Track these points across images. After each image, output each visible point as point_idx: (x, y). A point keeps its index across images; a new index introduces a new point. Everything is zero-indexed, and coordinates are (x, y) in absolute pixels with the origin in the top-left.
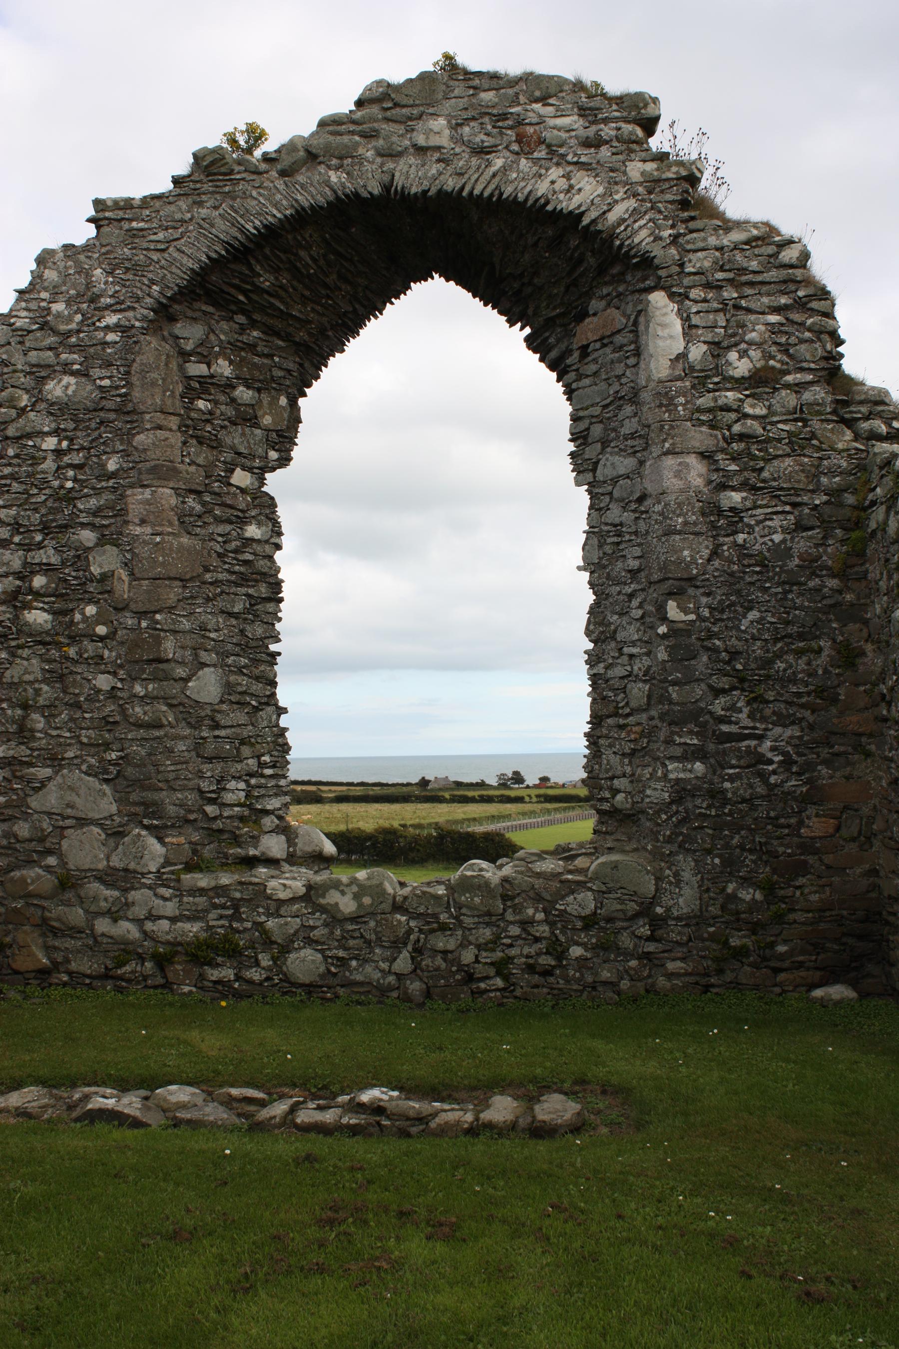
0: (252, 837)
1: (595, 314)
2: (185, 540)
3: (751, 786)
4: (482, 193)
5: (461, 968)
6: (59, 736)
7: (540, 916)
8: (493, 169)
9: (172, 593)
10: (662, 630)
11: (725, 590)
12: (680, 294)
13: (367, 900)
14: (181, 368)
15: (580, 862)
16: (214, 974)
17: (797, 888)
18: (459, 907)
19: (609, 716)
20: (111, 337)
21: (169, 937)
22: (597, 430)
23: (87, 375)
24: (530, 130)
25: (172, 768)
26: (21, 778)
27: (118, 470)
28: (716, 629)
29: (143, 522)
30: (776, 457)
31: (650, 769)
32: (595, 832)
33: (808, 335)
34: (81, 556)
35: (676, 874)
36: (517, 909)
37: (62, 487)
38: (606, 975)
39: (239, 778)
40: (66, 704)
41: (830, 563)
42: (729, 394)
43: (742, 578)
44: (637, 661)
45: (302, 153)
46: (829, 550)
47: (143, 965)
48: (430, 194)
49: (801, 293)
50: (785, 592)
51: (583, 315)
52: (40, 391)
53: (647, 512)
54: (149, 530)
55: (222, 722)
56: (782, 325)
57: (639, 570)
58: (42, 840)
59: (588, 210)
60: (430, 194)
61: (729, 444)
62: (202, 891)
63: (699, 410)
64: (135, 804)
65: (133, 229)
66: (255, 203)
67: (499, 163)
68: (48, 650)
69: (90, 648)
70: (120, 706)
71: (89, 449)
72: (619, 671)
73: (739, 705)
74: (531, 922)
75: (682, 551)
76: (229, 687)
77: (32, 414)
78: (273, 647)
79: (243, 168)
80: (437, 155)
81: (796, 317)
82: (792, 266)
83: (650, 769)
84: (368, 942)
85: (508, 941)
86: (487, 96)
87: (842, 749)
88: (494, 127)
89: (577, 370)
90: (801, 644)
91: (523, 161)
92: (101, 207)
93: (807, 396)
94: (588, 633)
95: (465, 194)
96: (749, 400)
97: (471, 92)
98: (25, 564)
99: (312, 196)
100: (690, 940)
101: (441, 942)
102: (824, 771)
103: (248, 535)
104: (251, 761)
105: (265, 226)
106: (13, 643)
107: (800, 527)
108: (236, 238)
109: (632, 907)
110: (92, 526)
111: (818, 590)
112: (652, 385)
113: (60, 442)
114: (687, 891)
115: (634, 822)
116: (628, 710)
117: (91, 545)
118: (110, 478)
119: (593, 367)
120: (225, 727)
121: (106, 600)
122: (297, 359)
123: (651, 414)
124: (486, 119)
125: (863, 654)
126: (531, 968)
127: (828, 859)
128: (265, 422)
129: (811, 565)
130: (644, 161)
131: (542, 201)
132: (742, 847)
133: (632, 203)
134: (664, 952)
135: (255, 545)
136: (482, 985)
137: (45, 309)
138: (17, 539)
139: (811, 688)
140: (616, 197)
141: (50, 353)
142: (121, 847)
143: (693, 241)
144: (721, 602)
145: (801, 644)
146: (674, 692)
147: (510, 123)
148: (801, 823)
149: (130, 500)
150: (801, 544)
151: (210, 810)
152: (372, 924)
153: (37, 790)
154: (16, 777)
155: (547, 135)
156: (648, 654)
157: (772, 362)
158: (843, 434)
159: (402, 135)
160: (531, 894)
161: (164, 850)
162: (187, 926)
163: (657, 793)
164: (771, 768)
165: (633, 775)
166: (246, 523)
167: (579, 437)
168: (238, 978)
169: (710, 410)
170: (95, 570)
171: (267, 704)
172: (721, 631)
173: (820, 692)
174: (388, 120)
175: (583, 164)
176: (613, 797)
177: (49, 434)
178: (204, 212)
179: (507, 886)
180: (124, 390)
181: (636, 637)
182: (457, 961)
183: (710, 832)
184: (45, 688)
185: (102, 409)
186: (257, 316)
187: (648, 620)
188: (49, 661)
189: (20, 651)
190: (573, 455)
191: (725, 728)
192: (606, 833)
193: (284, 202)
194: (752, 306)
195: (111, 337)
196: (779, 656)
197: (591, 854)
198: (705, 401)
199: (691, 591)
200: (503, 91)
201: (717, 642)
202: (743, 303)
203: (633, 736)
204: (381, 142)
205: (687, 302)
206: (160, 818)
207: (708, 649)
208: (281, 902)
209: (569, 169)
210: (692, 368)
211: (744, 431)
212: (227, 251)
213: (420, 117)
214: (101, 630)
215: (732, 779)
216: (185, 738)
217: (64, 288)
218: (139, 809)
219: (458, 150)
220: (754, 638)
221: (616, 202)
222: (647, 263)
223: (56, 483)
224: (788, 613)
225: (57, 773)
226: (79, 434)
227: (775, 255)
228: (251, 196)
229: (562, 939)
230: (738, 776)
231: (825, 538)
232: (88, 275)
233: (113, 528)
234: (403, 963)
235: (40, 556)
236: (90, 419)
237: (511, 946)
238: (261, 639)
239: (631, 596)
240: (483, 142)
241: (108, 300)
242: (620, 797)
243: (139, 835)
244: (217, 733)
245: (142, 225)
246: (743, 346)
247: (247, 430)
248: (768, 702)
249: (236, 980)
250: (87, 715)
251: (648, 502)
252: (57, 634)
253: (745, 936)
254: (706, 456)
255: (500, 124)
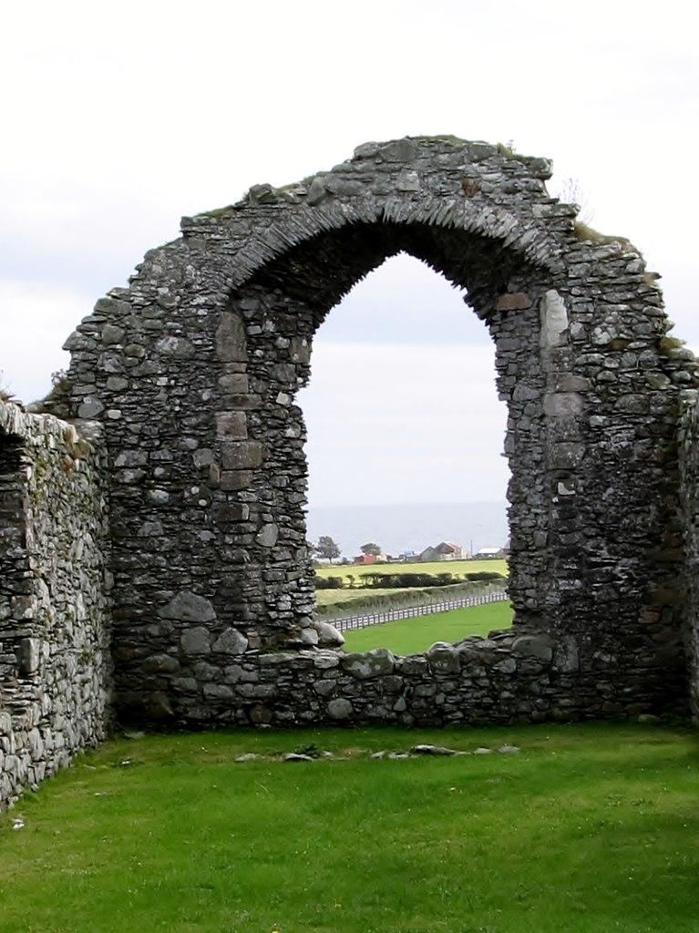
0: (297, 631)
1: (511, 293)
2: (253, 443)
3: (608, 594)
4: (441, 224)
5: (436, 706)
6: (177, 570)
7: (484, 674)
8: (448, 207)
9: (247, 478)
10: (555, 499)
11: (592, 476)
12: (565, 292)
13: (378, 667)
14: (246, 331)
15: (507, 641)
16: (282, 715)
17: (636, 654)
18: (434, 669)
19: (522, 551)
20: (201, 312)
21: (253, 694)
22: (513, 368)
23: (185, 337)
24: (471, 181)
25: (250, 589)
26: (151, 597)
27: (209, 399)
28: (587, 499)
29: (227, 433)
30: (624, 394)
31: (549, 584)
32: (514, 623)
33: (644, 318)
34: (188, 456)
35: (565, 647)
36: (469, 670)
37: (172, 410)
38: (524, 707)
39: (287, 593)
40: (181, 550)
41: (656, 459)
42: (596, 355)
43: (603, 468)
44: (540, 518)
45: (324, 192)
46: (655, 451)
47: (236, 712)
48: (408, 223)
49: (640, 291)
50: (629, 477)
51: (503, 290)
52: (154, 347)
53: (545, 426)
54: (231, 438)
55: (278, 558)
56: (629, 311)
57: (541, 461)
58: (166, 637)
59: (508, 235)
60: (408, 223)
61: (595, 386)
62: (273, 665)
63: (577, 365)
64: (228, 612)
65: (212, 239)
66: (293, 224)
67: (452, 202)
68: (167, 516)
69: (195, 514)
70: (217, 551)
71: (189, 385)
72: (530, 523)
73: (602, 545)
74: (478, 677)
75: (567, 451)
76: (280, 536)
77: (149, 361)
78: (303, 508)
79: (283, 200)
80: (411, 196)
81: (637, 306)
82: (634, 274)
83: (549, 584)
84: (378, 693)
85: (464, 690)
86: (444, 157)
87: (663, 571)
88: (448, 178)
89: (499, 325)
90: (638, 508)
91: (467, 202)
92: (189, 223)
93: (643, 356)
94: (508, 497)
95: (430, 224)
96: (607, 359)
97: (433, 155)
98: (149, 460)
99: (332, 222)
100: (573, 686)
101: (425, 691)
102: (652, 584)
103: (288, 435)
104: (294, 582)
105: (301, 241)
106: (144, 512)
107: (638, 437)
108: (282, 249)
109: (538, 667)
110: (192, 436)
111: (648, 475)
112: (548, 348)
113: (169, 381)
114: (571, 657)
115: (539, 616)
116: (534, 548)
117: (193, 448)
118: (205, 405)
119: (511, 327)
120: (279, 561)
121: (204, 483)
122: (311, 312)
123: (549, 367)
124: (443, 173)
125: (675, 514)
126: (478, 705)
127: (655, 636)
128: (294, 359)
129: (644, 460)
130: (543, 204)
131: (480, 230)
132: (603, 630)
133: (536, 232)
134: (558, 693)
135: (292, 442)
136: (449, 717)
137: (154, 291)
138: (143, 444)
139: (645, 534)
140: (526, 227)
141: (159, 321)
142: (219, 639)
143: (575, 257)
144: (590, 483)
145: (638, 508)
146: (563, 538)
147: (458, 176)
148: (639, 616)
149: (218, 419)
150: (639, 448)
151: (273, 614)
152: (381, 682)
153: (162, 605)
154: (148, 597)
155: (483, 185)
156: (547, 513)
157: (622, 335)
158: (665, 380)
159: (389, 182)
160: (478, 661)
161: (247, 640)
162: (264, 687)
163: (553, 598)
164: (620, 582)
165: (537, 587)
166: (286, 428)
167: (502, 369)
168: (297, 718)
169: (583, 365)
170: (198, 465)
171: (302, 545)
172: (590, 501)
173: (649, 536)
174: (379, 171)
175: (505, 205)
176: (526, 601)
177: (161, 375)
178: (259, 229)
179: (463, 656)
180: (211, 348)
181: (539, 503)
182: (434, 703)
183: (585, 621)
184: (166, 540)
185: (196, 360)
186: (289, 289)
187: (547, 492)
188: (168, 523)
189: (148, 517)
190: (498, 380)
191: (593, 559)
192: (522, 623)
193: (313, 225)
194: (609, 299)
195: (201, 312)
196: (625, 515)
197: (512, 636)
198: (581, 359)
199: (573, 476)
200: (454, 154)
201: (589, 508)
202: (604, 297)
203: (538, 564)
204: (375, 186)
205: (570, 296)
206: (243, 621)
207: (583, 512)
208: (324, 670)
209: (497, 208)
210: (573, 339)
211: (605, 378)
212: (275, 256)
213: (399, 170)
214: (203, 502)
215: (597, 589)
216: (256, 570)
217: (167, 278)
218: (231, 615)
219: (425, 194)
220: (611, 505)
221: (526, 230)
222: (545, 269)
223: (168, 408)
224: (630, 490)
225: (176, 594)
226: (181, 375)
227: (625, 267)
228: (291, 220)
229: (497, 687)
230: (601, 588)
231: (653, 444)
232: (183, 270)
233: (208, 438)
234: (401, 704)
235: (157, 455)
236: (189, 366)
237: (465, 692)
238: (297, 503)
239: (536, 477)
240: (441, 189)
241: (198, 287)
242: (530, 601)
243: (231, 632)
244: (274, 565)
245: (218, 237)
246: (605, 324)
247: (285, 366)
248: (618, 543)
249: (295, 719)
250: (195, 557)
251: (546, 420)
252: (172, 506)
253: (605, 683)
254: (582, 394)
255: (452, 177)
